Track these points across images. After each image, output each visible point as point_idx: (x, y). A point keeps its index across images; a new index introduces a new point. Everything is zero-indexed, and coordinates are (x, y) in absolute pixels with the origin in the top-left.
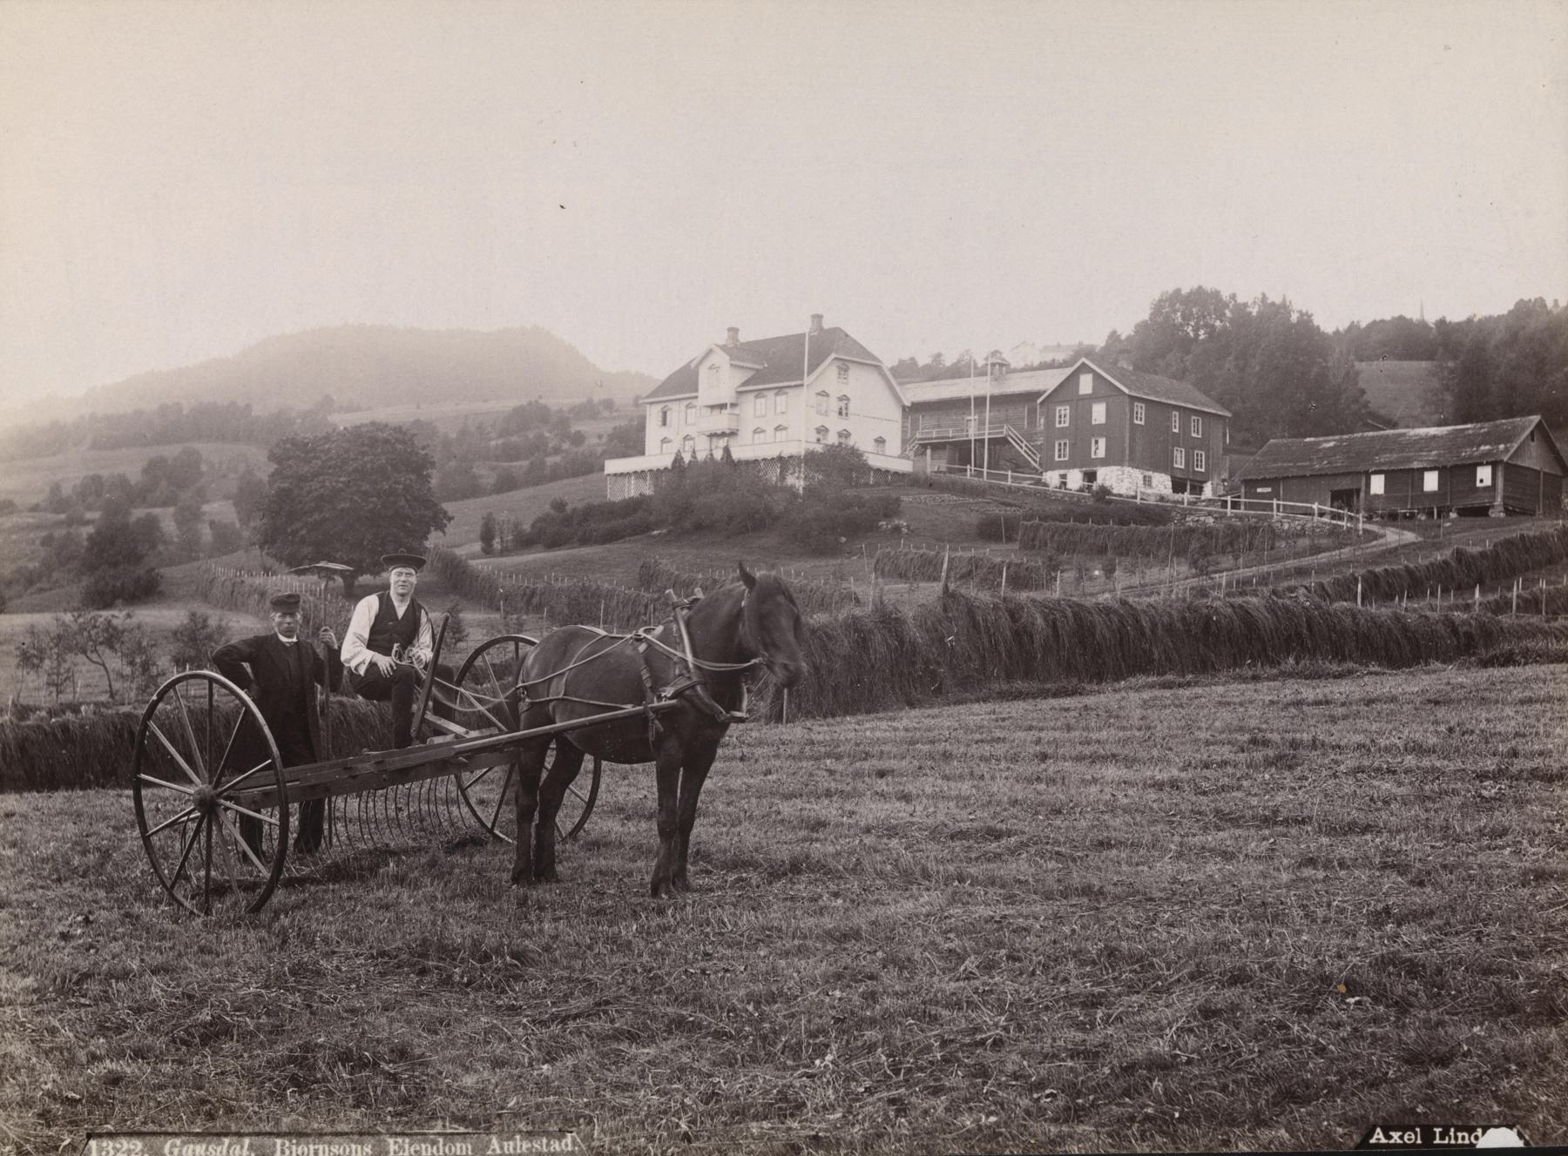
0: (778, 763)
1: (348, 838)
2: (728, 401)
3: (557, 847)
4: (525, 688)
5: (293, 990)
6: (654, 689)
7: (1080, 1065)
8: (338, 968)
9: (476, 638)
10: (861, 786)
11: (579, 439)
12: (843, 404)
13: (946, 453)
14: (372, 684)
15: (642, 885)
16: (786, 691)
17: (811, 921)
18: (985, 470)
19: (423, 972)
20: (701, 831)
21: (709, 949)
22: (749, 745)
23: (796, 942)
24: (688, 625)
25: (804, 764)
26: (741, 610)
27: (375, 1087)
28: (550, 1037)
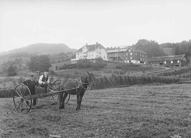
7: (128, 131)
19: (48, 119)
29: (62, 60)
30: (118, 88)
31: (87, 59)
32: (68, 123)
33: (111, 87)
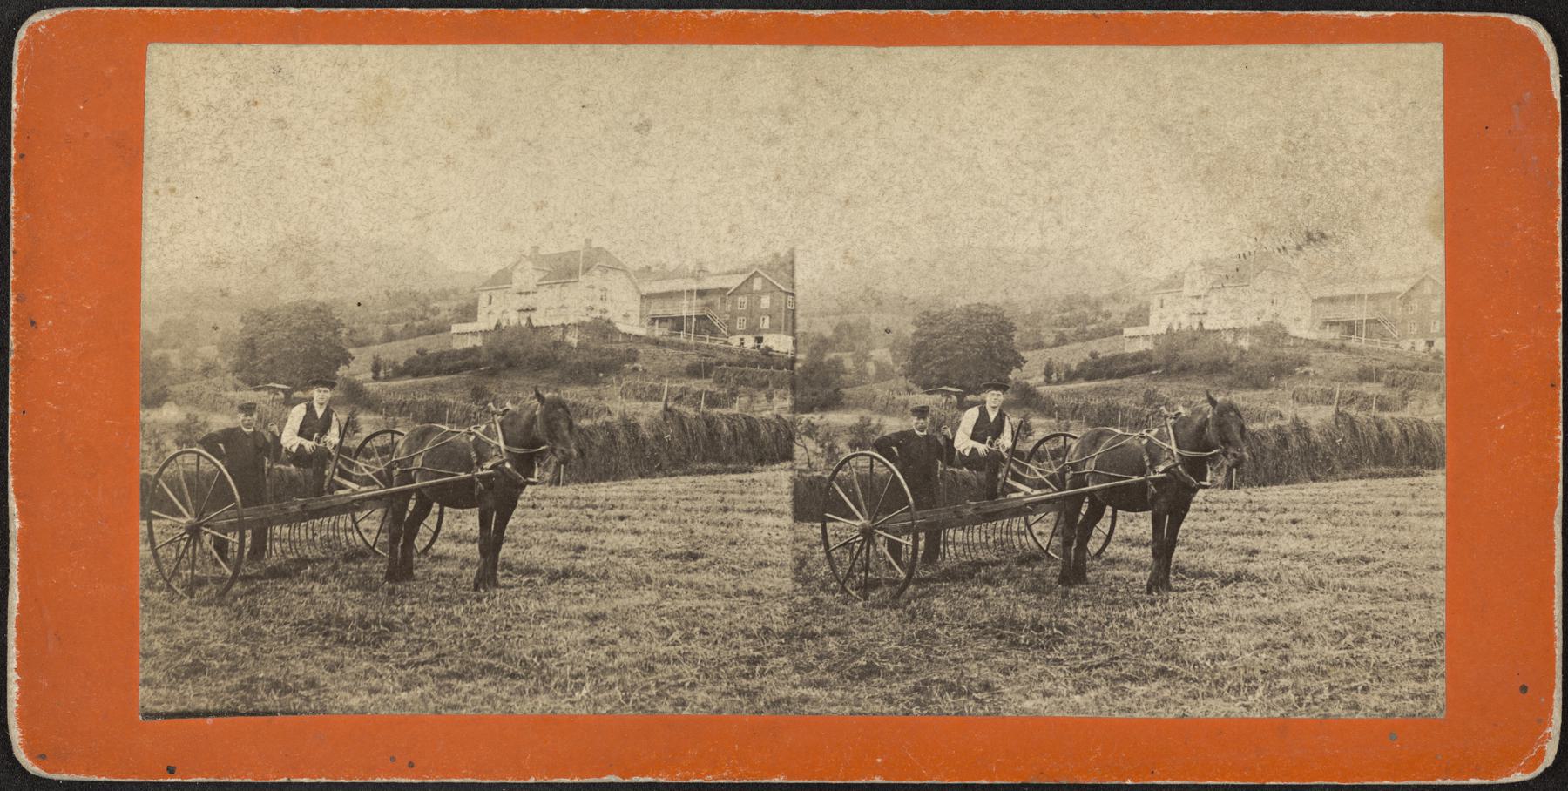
0: (556, 510)
1: (956, 554)
2: (531, 290)
3: (415, 559)
5: (918, 647)
6: (479, 464)
7: (1418, 703)
8: (947, 634)
10: (608, 525)
11: (436, 312)
12: (603, 293)
15: (467, 583)
17: (575, 608)
18: (1363, 339)
19: (326, 634)
20: (506, 550)
21: (1183, 626)
22: (538, 499)
23: (565, 620)
24: (1174, 428)
27: (969, 707)
28: (407, 676)
29: (1078, 332)
30: (1364, 481)
32: (1103, 658)
33: (1332, 474)
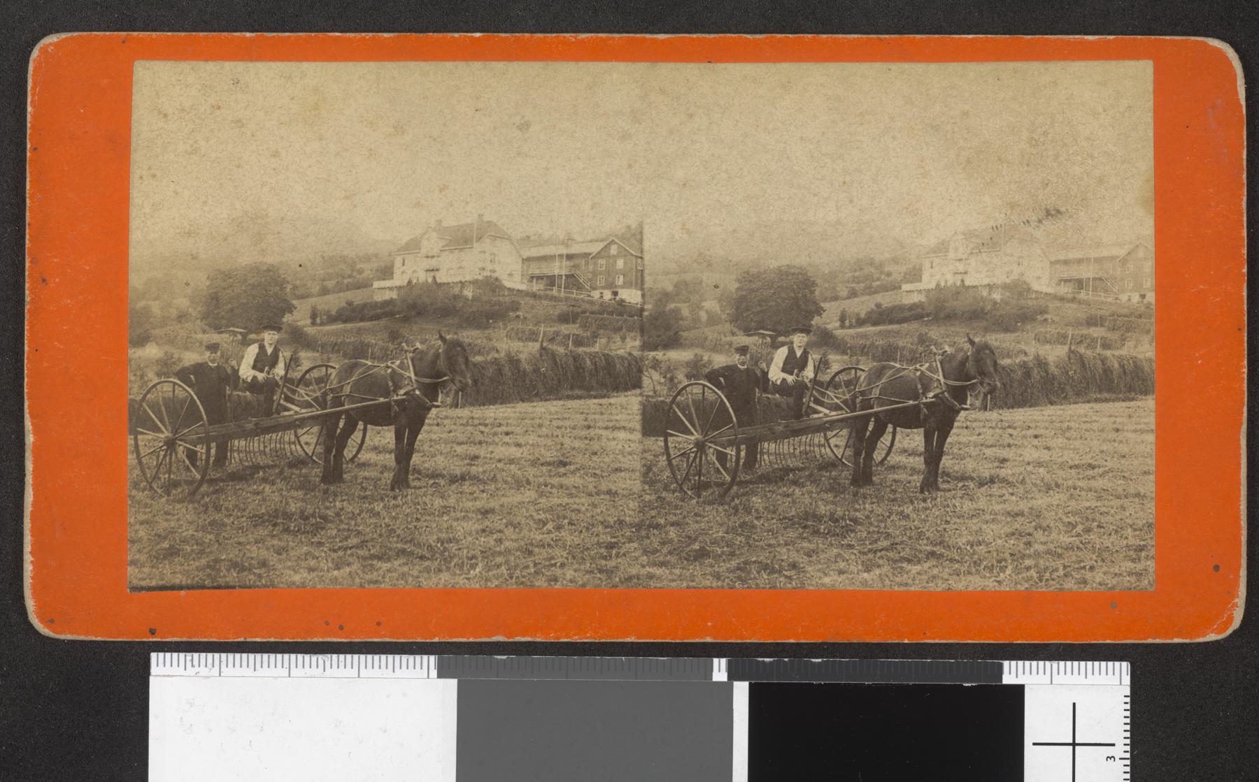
0: (455, 427)
3: (344, 466)
4: (330, 389)
5: (740, 535)
7: (1133, 579)
8: (763, 525)
9: (306, 365)
10: (496, 439)
11: (360, 272)
13: (544, 282)
14: (783, 388)
16: (460, 393)
17: (470, 504)
19: (275, 525)
20: (416, 459)
21: (948, 519)
23: (463, 514)
25: (469, 428)
26: (968, 357)
27: (780, 582)
29: (866, 288)
30: (1091, 405)
31: (967, 283)
32: (886, 543)
